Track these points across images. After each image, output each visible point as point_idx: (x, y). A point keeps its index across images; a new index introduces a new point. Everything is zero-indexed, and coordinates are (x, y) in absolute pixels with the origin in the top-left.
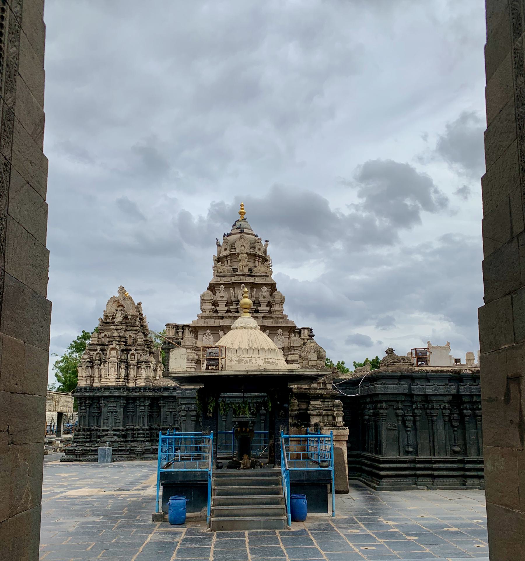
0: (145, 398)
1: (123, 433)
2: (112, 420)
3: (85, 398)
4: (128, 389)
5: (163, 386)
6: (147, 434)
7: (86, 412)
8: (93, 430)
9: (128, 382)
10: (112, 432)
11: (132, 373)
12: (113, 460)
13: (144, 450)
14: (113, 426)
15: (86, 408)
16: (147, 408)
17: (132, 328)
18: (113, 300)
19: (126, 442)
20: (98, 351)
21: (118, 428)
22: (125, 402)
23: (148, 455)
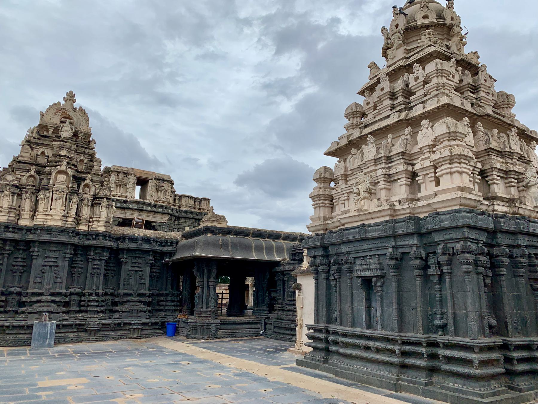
0: (103, 248)
1: (67, 299)
4: (77, 233)
5: (128, 234)
6: (102, 301)
8: (11, 293)
9: (78, 224)
10: (49, 298)
11: (86, 211)
12: (58, 342)
14: (50, 289)
15: (4, 258)
16: (103, 264)
17: (84, 150)
18: (56, 108)
20: (32, 173)
21: (142, 292)
22: (73, 252)
23: (106, 333)
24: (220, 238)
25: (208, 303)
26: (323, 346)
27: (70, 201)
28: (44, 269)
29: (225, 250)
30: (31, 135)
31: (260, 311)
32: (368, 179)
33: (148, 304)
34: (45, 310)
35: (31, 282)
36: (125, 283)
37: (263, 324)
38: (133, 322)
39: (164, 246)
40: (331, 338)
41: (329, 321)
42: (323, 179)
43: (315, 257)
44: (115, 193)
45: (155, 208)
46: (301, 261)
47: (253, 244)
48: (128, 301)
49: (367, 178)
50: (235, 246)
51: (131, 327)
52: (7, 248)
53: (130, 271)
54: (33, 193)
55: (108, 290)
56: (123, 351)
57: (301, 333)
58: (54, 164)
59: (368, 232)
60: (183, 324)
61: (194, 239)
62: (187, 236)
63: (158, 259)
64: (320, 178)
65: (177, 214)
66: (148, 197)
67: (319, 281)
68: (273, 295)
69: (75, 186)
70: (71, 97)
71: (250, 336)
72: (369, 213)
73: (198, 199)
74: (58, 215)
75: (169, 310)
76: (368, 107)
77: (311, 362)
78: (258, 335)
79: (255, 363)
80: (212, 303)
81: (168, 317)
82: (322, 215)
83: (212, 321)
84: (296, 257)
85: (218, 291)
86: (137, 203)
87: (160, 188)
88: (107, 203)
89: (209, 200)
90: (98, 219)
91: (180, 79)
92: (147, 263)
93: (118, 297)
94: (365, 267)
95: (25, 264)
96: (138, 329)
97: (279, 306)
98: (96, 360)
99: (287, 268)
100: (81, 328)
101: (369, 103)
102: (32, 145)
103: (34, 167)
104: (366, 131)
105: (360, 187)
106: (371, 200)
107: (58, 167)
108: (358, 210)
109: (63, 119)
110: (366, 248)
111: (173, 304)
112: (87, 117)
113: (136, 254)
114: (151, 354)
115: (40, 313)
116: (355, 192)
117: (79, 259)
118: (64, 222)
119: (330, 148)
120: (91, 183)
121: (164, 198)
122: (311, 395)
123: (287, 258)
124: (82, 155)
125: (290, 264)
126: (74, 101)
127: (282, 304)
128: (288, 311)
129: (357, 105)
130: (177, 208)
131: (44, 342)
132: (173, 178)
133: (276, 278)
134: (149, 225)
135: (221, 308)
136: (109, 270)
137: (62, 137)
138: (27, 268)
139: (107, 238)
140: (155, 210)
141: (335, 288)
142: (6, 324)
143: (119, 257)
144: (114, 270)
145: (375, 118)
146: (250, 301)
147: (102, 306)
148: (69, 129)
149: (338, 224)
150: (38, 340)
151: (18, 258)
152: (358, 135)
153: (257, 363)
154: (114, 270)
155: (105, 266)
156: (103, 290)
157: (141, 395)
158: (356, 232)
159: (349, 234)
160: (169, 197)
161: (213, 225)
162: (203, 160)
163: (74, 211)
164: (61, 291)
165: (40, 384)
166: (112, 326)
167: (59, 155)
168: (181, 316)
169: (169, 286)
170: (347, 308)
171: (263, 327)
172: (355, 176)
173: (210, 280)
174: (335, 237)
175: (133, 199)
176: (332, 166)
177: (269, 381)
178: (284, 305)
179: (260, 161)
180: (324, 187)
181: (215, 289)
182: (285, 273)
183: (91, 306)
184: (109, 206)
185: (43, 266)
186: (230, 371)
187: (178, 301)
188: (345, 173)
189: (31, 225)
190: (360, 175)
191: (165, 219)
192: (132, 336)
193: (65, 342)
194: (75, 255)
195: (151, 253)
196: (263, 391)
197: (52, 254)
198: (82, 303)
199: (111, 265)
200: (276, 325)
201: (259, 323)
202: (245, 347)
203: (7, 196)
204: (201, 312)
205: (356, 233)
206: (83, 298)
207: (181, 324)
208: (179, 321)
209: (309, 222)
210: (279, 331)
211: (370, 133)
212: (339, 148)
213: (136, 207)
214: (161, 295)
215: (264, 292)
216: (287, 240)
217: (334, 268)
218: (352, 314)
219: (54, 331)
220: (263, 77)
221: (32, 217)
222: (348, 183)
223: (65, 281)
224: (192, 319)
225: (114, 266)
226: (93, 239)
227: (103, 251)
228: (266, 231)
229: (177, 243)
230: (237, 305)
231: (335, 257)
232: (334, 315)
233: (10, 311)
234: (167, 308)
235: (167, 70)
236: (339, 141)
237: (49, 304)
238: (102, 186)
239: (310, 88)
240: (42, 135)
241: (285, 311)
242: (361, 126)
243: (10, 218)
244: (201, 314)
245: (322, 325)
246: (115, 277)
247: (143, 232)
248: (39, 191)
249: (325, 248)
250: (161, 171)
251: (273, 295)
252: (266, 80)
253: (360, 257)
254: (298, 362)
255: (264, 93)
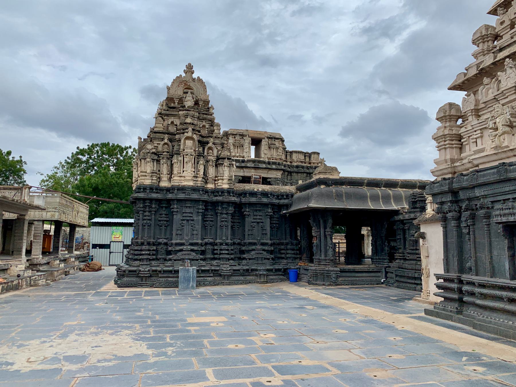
0: (229, 203)
1: (203, 248)
2: (187, 230)
3: (151, 200)
6: (232, 250)
7: (150, 220)
8: (160, 244)
9: (206, 183)
11: (212, 171)
12: (199, 284)
13: (232, 271)
16: (230, 217)
17: (205, 116)
18: (178, 80)
19: (204, 260)
20: (166, 141)
21: (195, 241)
22: (204, 208)
23: (237, 278)
24: (333, 189)
25: (326, 251)
26: (456, 296)
27: (198, 163)
28: (182, 223)
29: (339, 200)
30: (162, 108)
31: (380, 260)
32: (507, 110)
33: (271, 252)
34: (187, 257)
35: (174, 235)
36: (249, 233)
37: (384, 273)
38: (259, 268)
39: (281, 199)
40: (465, 288)
41: (462, 270)
42: (448, 117)
43: (442, 203)
44: (233, 154)
45: (269, 165)
46: (423, 209)
47: (368, 194)
48: (253, 250)
49: (507, 110)
50: (349, 196)
51: (257, 273)
52: (153, 206)
53: (253, 222)
54: (168, 159)
55: (235, 240)
56: (253, 294)
57: (427, 283)
58: (182, 131)
59: (510, 172)
60: (304, 271)
61: (308, 191)
62: (301, 189)
63: (276, 212)
64: (445, 116)
65: (289, 170)
66: (263, 156)
67: (448, 229)
68: (393, 244)
69: (201, 149)
70: (190, 69)
71: (371, 284)
72: (511, 150)
73: (308, 153)
74: (189, 176)
75: (290, 258)
76: (503, 27)
77: (443, 312)
78: (379, 283)
79: (380, 311)
80: (330, 252)
81: (289, 264)
82: (448, 157)
83: (332, 269)
84: (418, 205)
85: (334, 241)
86: (253, 161)
87: (272, 146)
88: (229, 163)
89: (318, 154)
90: (222, 178)
91: (279, 39)
92: (267, 215)
93: (244, 246)
94: (507, 211)
95: (168, 219)
96: (264, 275)
97: (401, 255)
98: (231, 301)
99: (407, 216)
100: (216, 273)
101: (504, 21)
102: (163, 117)
103: (167, 135)
104: (501, 55)
105: (498, 120)
106: (513, 135)
107: (186, 134)
108: (496, 148)
109: (185, 90)
110: (508, 190)
111: (293, 252)
112: (205, 86)
113: (257, 207)
114: (277, 297)
115: (183, 260)
116: (491, 127)
117: (210, 213)
118: (195, 182)
119: (456, 81)
120: (213, 146)
121: (276, 155)
122: (446, 346)
123: (407, 206)
124: (204, 121)
125: (410, 212)
126: (193, 73)
127: (404, 253)
128: (411, 260)
129: (487, 27)
130: (289, 164)
131: (188, 285)
132: (283, 136)
133: (395, 227)
134: (265, 181)
135: (339, 257)
136: (235, 222)
137: (186, 107)
138: (170, 222)
139: (231, 194)
140: (269, 166)
141: (467, 236)
142: (159, 269)
143: (243, 210)
144: (239, 223)
145: (512, 38)
146: (368, 250)
147: (232, 254)
148: (191, 98)
149: (470, 165)
150: (183, 282)
151: (162, 214)
152: (492, 61)
153: (383, 311)
154: (239, 223)
155: (231, 219)
156: (231, 240)
157: (273, 335)
158: (494, 173)
159: (484, 176)
160: (281, 154)
161: (326, 176)
162: (308, 116)
163: (202, 172)
164: (198, 241)
165: (189, 320)
166: (241, 271)
167: (185, 123)
168: (301, 264)
169: (288, 236)
170: (484, 257)
171: (384, 275)
172: (489, 110)
173: (326, 230)
174: (467, 180)
175: (249, 158)
176: (459, 102)
177: (397, 329)
178: (406, 255)
179: (364, 110)
180: (450, 126)
181: (331, 239)
182: (405, 221)
183: (223, 254)
184: (231, 165)
185: (182, 220)
186: (355, 318)
187: (297, 250)
188: (476, 107)
189: (170, 186)
190: (497, 107)
191: (278, 175)
192: (259, 280)
193: (205, 285)
194: (206, 210)
195: (270, 206)
196: (392, 339)
197: (188, 210)
198: (215, 252)
199: (236, 217)
200: (398, 274)
201: (379, 272)
202: (366, 294)
203: (149, 162)
204: (320, 261)
205: (494, 173)
206: (216, 247)
207: (302, 271)
208: (300, 268)
209: (433, 166)
210: (402, 280)
211: (508, 57)
212: (467, 80)
213: (253, 166)
214: (282, 244)
215: (382, 242)
216: (406, 188)
217: (465, 215)
218: (491, 263)
219: (195, 275)
220: (362, 22)
221: (170, 179)
222: (481, 118)
223: (200, 233)
224: (312, 267)
225: (238, 219)
226: (220, 196)
227: (229, 206)
228: (381, 180)
229: (292, 196)
230: (354, 253)
231: (467, 202)
232: (468, 265)
233: (160, 258)
234: (288, 256)
235: (266, 31)
236: (466, 72)
237: (189, 252)
238: (223, 148)
239: (416, 24)
240: (171, 107)
241: (408, 260)
242: (495, 50)
243: (153, 181)
244: (320, 262)
245: (453, 275)
246: (241, 228)
247: (261, 187)
248: (173, 156)
249: (454, 193)
250: (270, 130)
251: (393, 244)
252: (366, 24)
253: (500, 201)
254: (427, 312)
255: (364, 39)
